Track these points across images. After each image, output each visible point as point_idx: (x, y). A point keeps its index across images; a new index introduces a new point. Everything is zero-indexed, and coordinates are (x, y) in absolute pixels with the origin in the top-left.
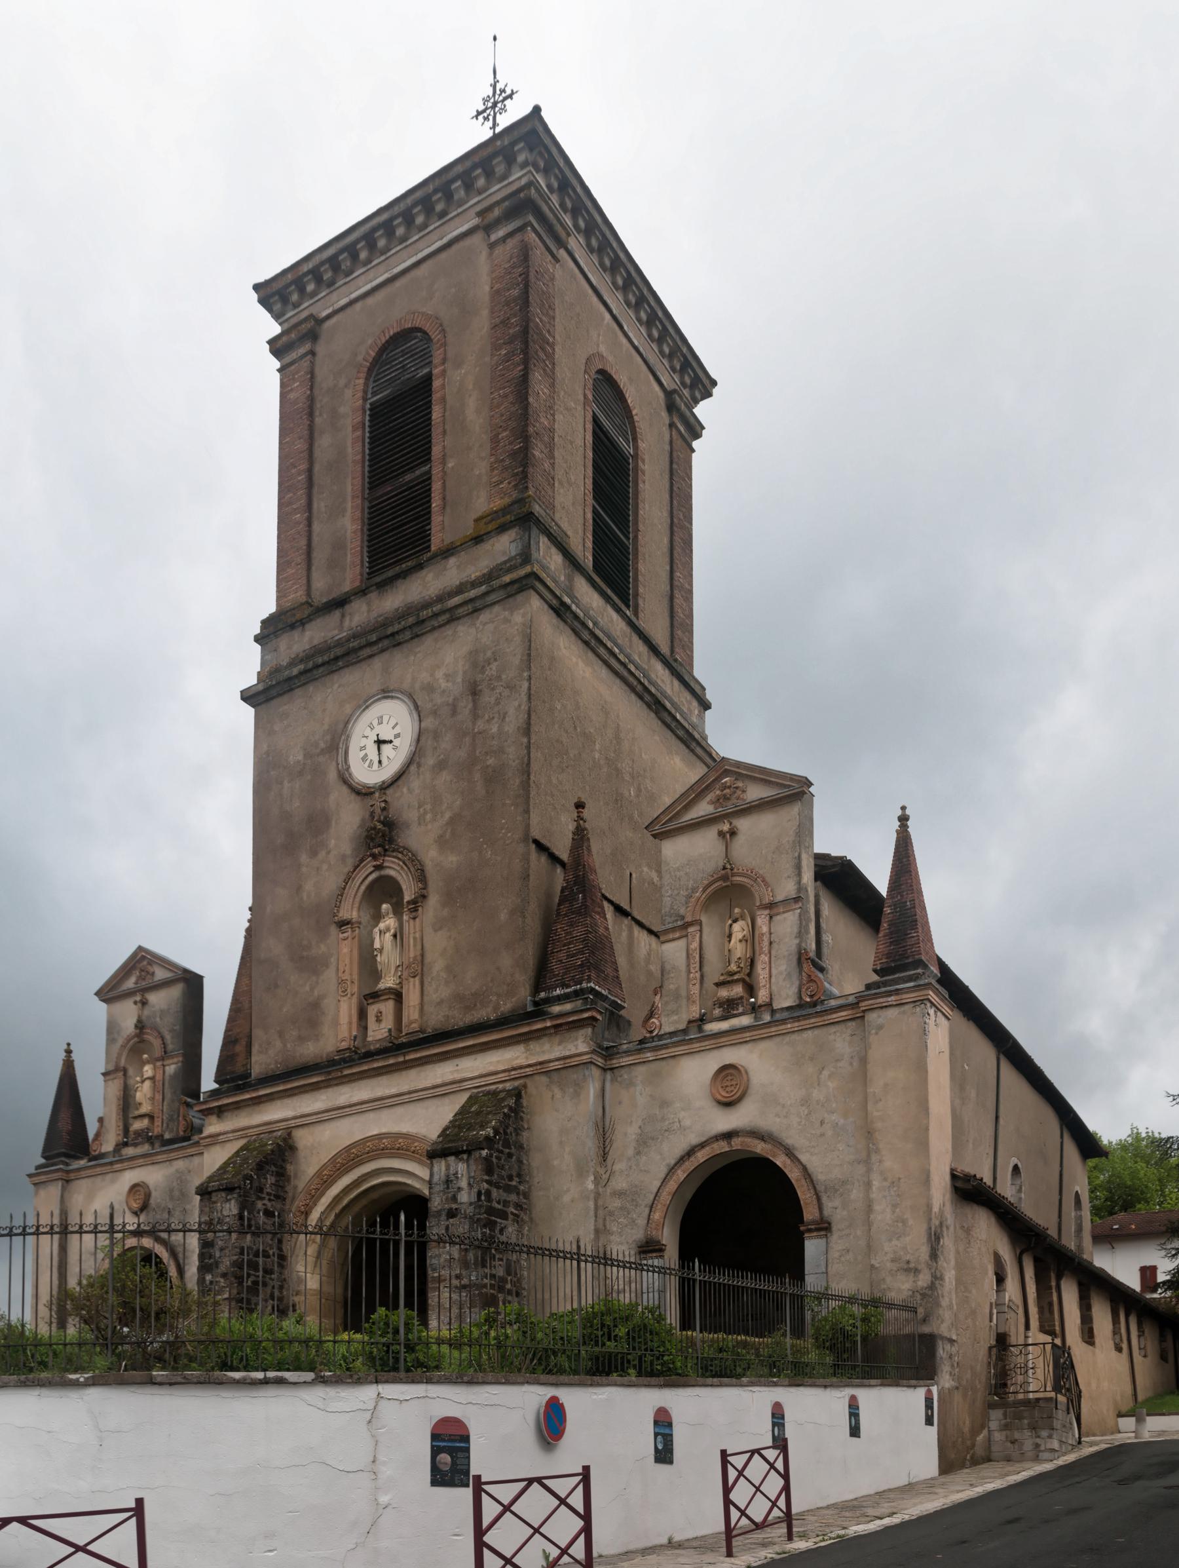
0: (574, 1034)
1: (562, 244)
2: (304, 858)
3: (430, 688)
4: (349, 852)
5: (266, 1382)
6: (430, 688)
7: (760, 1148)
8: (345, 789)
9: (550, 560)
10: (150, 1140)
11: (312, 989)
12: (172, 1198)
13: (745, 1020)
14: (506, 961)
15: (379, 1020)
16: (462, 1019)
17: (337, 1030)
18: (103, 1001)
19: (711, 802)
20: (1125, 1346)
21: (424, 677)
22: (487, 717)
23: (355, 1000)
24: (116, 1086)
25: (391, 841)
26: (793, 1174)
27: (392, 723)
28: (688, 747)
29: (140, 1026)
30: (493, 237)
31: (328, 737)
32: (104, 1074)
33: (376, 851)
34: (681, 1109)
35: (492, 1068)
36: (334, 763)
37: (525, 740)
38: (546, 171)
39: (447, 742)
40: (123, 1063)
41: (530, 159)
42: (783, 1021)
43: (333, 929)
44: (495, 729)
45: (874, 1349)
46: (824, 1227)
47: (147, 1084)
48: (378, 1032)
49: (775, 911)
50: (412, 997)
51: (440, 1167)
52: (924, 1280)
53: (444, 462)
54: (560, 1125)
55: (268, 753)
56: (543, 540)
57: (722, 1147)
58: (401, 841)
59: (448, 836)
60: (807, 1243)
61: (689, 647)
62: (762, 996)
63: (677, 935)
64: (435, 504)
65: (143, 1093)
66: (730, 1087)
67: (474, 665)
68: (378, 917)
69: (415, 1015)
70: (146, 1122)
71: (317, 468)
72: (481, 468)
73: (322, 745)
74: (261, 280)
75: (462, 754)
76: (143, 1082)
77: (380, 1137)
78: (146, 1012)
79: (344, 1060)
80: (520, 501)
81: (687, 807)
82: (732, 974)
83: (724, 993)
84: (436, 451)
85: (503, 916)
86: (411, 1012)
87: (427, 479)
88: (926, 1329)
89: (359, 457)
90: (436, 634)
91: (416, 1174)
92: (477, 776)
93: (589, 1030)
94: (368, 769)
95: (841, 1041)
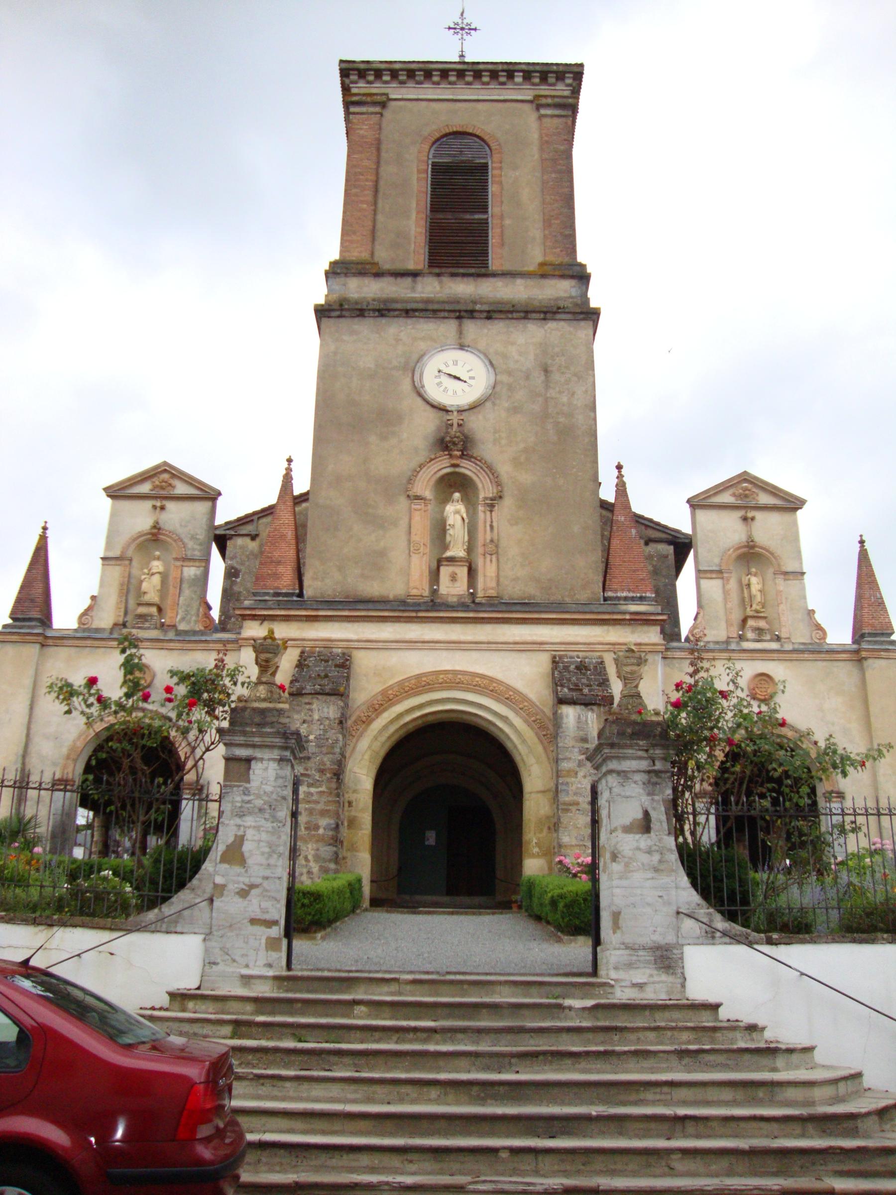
2: (373, 439)
3: (505, 356)
8: (419, 401)
13: (774, 646)
17: (407, 576)
18: (108, 496)
19: (734, 495)
22: (557, 389)
24: (116, 572)
29: (156, 527)
32: (102, 558)
40: (130, 553)
43: (403, 502)
44: (565, 399)
49: (787, 577)
53: (502, 217)
55: (335, 353)
59: (522, 459)
63: (714, 576)
71: (382, 183)
73: (395, 363)
74: (344, 59)
75: (537, 407)
77: (455, 672)
81: (131, 485)
85: (576, 529)
90: (507, 322)
92: (549, 426)
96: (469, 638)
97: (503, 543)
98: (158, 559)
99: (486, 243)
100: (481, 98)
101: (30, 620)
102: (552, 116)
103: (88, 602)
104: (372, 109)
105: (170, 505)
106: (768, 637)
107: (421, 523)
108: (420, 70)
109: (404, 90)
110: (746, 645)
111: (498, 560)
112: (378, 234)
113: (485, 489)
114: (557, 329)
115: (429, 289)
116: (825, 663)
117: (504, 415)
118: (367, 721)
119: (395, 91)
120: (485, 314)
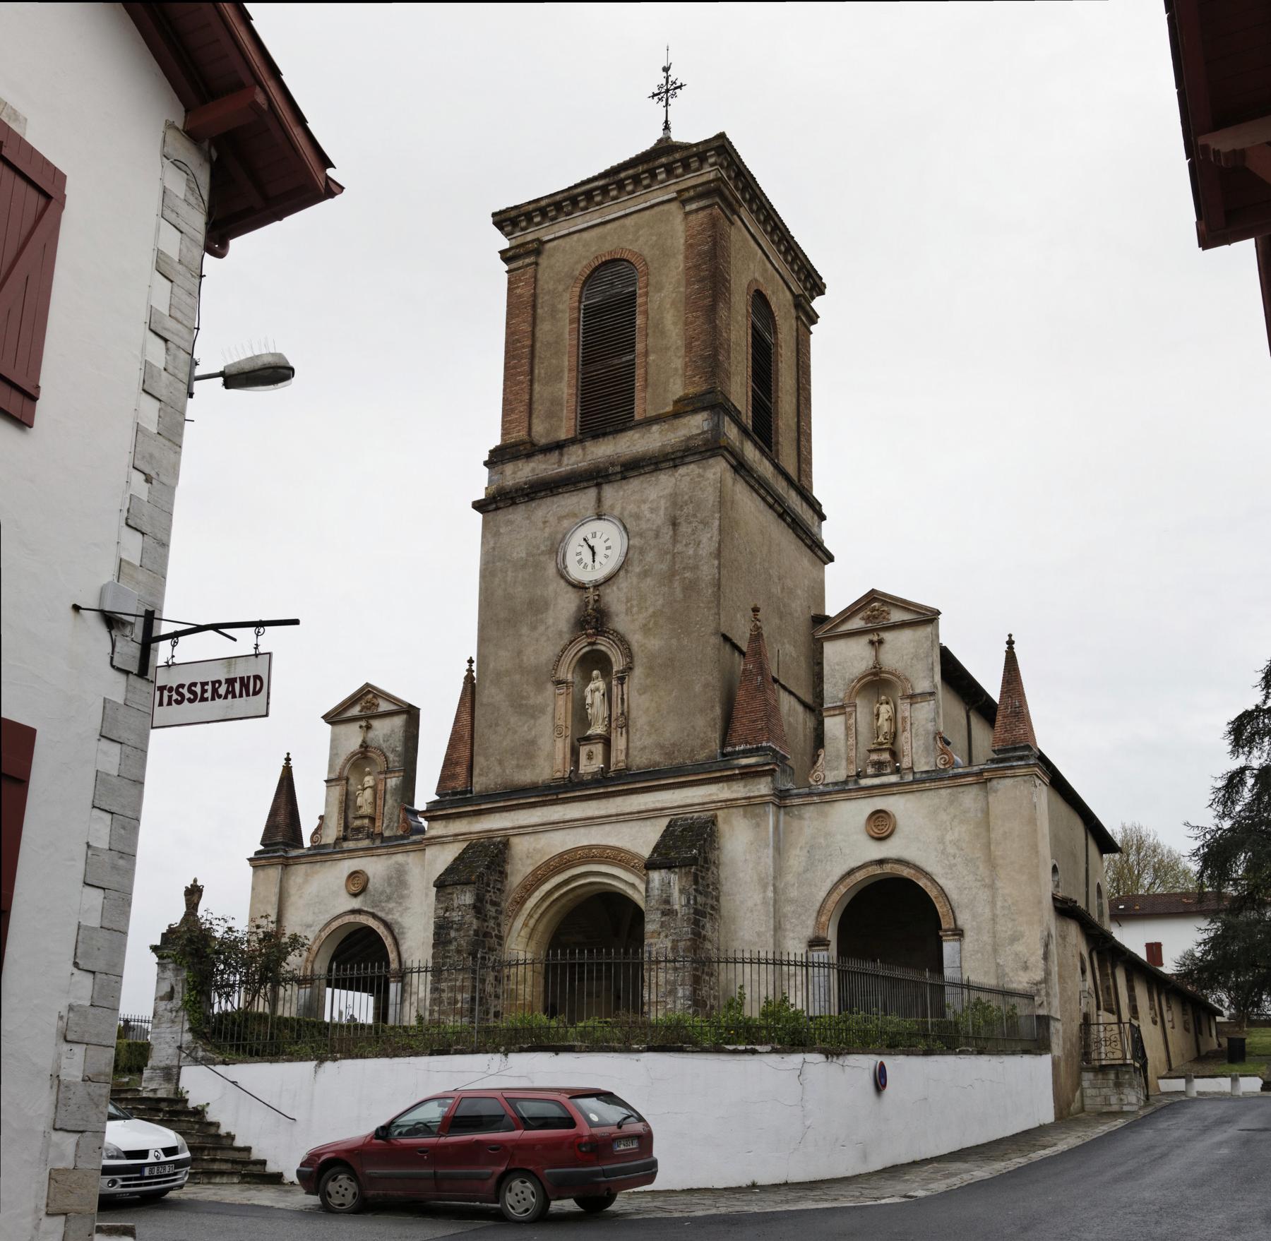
0: (757, 780)
1: (734, 212)
2: (524, 630)
3: (637, 517)
4: (565, 629)
5: (745, 1052)
6: (637, 517)
7: (906, 872)
8: (562, 583)
9: (732, 432)
10: (371, 836)
11: (530, 729)
12: (390, 885)
13: (894, 779)
14: (700, 722)
15: (590, 756)
16: (664, 763)
17: (550, 761)
19: (862, 619)
20: (1158, 1019)
21: (632, 508)
23: (568, 740)
24: (337, 791)
25: (602, 624)
26: (932, 893)
27: (605, 538)
28: (812, 551)
29: (365, 746)
30: (688, 208)
31: (548, 543)
33: (590, 631)
34: (840, 842)
35: (689, 801)
36: (554, 563)
37: (716, 562)
38: (727, 169)
39: (651, 557)
41: (719, 161)
42: (923, 781)
43: (550, 687)
44: (691, 552)
45: (1002, 1028)
46: (959, 933)
47: (369, 792)
48: (590, 765)
50: (619, 743)
51: (656, 876)
52: (1038, 975)
53: (646, 354)
54: (741, 844)
55: (494, 548)
56: (727, 419)
57: (877, 870)
58: (611, 626)
59: (651, 625)
60: (945, 944)
61: (809, 475)
62: (906, 763)
64: (638, 384)
65: (364, 800)
66: (881, 826)
67: (674, 504)
68: (588, 679)
69: (623, 757)
70: (366, 821)
71: (538, 345)
72: (678, 363)
73: (543, 548)
75: (664, 567)
76: (364, 789)
77: (590, 847)
78: (371, 734)
79: (558, 787)
80: (711, 391)
82: (881, 744)
83: (874, 757)
84: (639, 347)
85: (698, 688)
86: (618, 757)
87: (632, 364)
88: (1041, 1012)
89: (575, 342)
90: (641, 478)
91: (627, 882)
92: (676, 584)
93: (769, 779)
94: (584, 570)
95: (970, 798)
96: (603, 813)
97: (633, 714)
98: (369, 774)
99: (632, 389)
100: (628, 211)
101: (276, 844)
102: (697, 211)
103: (317, 822)
104: (528, 261)
105: (376, 723)
106: (889, 770)
107: (562, 706)
108: (565, 200)
109: (556, 227)
110: (865, 782)
111: (627, 732)
112: (535, 406)
113: (618, 663)
114: (688, 474)
115: (573, 459)
116: (949, 791)
117: (635, 580)
118: (521, 902)
119: (546, 232)
120: (619, 476)
